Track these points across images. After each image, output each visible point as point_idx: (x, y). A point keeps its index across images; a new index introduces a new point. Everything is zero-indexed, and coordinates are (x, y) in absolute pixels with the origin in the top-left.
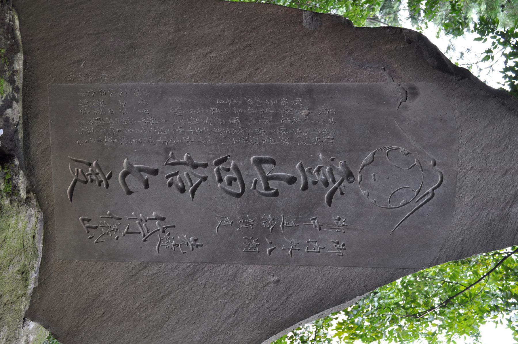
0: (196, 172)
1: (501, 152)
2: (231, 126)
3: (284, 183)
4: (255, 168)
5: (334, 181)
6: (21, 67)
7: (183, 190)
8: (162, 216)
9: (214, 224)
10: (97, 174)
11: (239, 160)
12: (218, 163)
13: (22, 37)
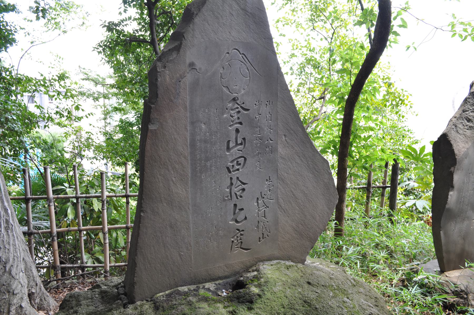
0: (234, 184)
1: (222, 17)
2: (211, 166)
3: (239, 135)
4: (232, 151)
5: (237, 108)
6: (185, 287)
7: (243, 190)
8: (256, 199)
9: (259, 171)
10: (237, 237)
11: (228, 160)
12: (230, 172)
13: (168, 290)
